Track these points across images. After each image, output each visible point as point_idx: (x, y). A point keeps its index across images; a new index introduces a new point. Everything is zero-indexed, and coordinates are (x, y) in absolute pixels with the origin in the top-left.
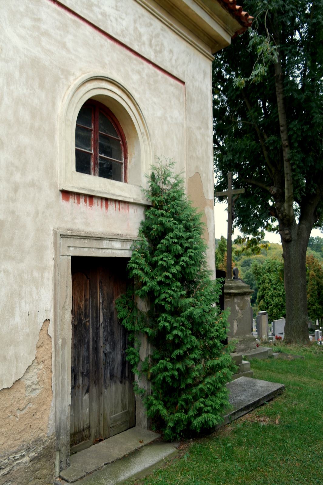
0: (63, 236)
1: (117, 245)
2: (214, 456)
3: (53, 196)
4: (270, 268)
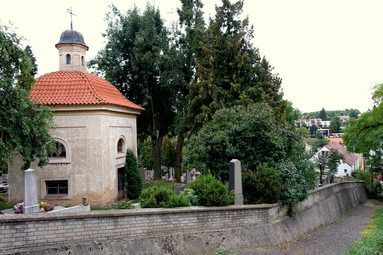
1: (123, 165)
2: (206, 96)
3: (115, 159)
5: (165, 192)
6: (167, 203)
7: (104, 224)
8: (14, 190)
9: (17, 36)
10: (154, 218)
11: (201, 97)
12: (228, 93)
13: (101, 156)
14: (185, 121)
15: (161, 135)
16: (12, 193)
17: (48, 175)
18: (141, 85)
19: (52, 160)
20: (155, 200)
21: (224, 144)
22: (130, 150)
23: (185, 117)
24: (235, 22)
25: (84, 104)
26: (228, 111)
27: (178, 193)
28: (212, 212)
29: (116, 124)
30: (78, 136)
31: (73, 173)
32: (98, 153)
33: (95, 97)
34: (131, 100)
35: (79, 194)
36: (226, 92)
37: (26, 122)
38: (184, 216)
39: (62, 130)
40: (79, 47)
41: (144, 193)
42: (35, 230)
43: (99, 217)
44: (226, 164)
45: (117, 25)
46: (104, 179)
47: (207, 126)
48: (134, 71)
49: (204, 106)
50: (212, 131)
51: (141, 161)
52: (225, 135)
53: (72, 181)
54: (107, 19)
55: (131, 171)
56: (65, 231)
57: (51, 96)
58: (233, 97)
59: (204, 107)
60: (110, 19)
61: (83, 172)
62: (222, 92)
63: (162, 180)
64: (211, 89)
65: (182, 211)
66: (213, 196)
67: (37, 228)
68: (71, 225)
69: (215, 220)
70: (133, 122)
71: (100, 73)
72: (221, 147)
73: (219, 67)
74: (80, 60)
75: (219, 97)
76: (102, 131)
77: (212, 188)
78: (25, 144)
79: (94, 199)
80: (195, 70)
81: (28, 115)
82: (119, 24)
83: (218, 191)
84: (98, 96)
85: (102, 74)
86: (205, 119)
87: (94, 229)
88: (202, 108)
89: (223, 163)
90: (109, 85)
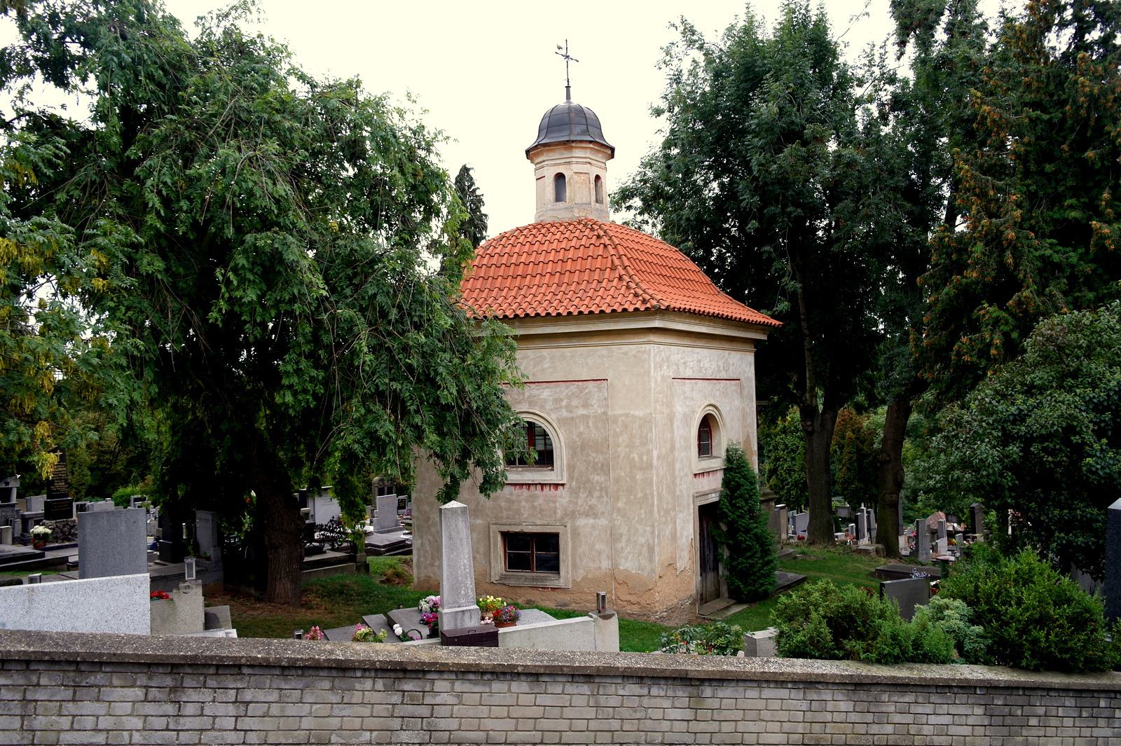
1: (713, 495)
2: (993, 274)
3: (691, 476)
5: (863, 604)
6: (868, 645)
7: (658, 699)
9: (425, 133)
10: (827, 695)
11: (975, 275)
12: (1080, 259)
13: (649, 466)
14: (916, 360)
15: (832, 405)
16: (422, 559)
18: (767, 248)
19: (515, 475)
20: (825, 630)
21: (1076, 439)
22: (737, 450)
23: (916, 346)
24: (1106, 7)
25: (602, 312)
26: (1087, 322)
27: (908, 614)
28: (1045, 693)
30: (586, 405)
31: (573, 515)
32: (641, 459)
33: (632, 291)
34: (737, 295)
36: (1071, 254)
37: (446, 367)
38: (934, 698)
40: (589, 151)
42: (455, 701)
43: (641, 678)
44: (1083, 512)
45: (696, 76)
46: (659, 536)
47: (1005, 374)
48: (745, 208)
49: (986, 305)
50: (1023, 393)
51: (768, 481)
52: (1076, 407)
54: (665, 62)
55: (741, 517)
56: (537, 712)
57: (513, 293)
58: (1100, 271)
59: (988, 311)
60: (675, 62)
62: (1055, 255)
63: (834, 544)
64: (1015, 248)
65: (925, 679)
66: (1048, 634)
67: (459, 695)
68: (554, 694)
69: (1054, 722)
70: (743, 364)
71: (647, 222)
72: (1060, 450)
73: (1043, 169)
75: (1045, 275)
77: (1039, 602)
78: (445, 430)
80: (946, 191)
81: (452, 349)
82: (701, 75)
83: (1067, 617)
84: (641, 288)
85: (653, 227)
86: (993, 351)
87: (626, 713)
88: (977, 313)
89: (1071, 508)
90: (673, 255)
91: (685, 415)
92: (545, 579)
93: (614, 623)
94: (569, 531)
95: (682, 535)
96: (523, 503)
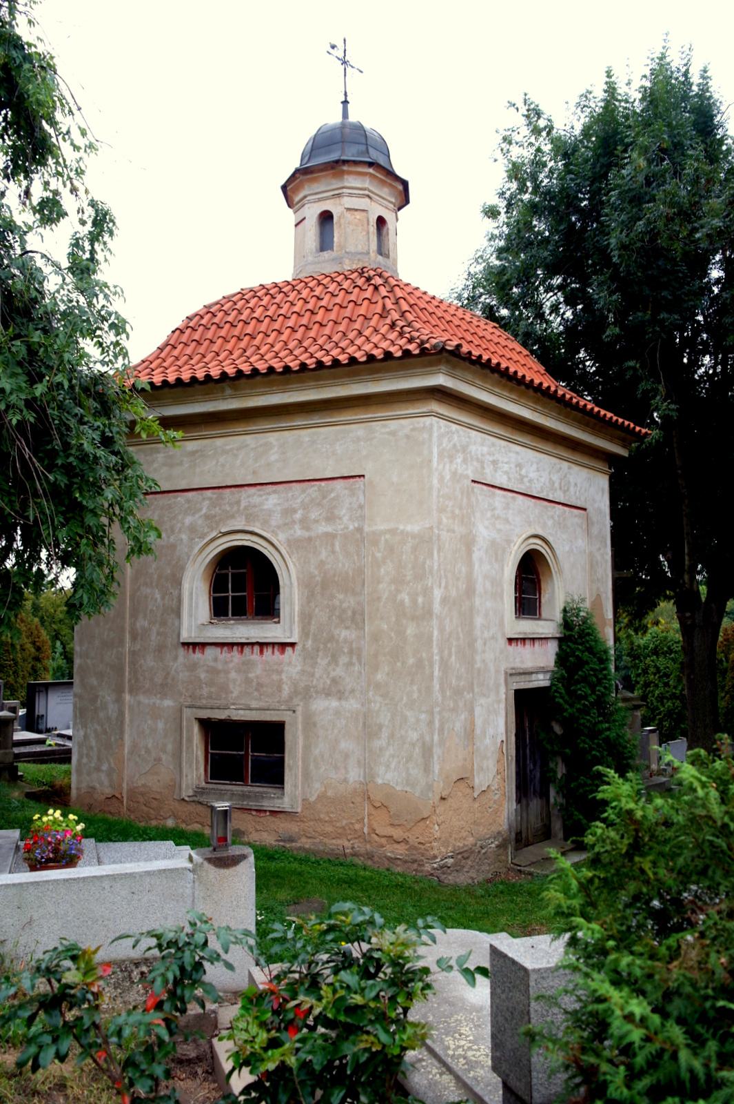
0: (511, 675)
1: (541, 676)
3: (502, 642)
4: (656, 647)
8: (91, 748)
13: (428, 613)
16: (85, 760)
17: (210, 697)
29: (509, 478)
30: (331, 518)
31: (307, 694)
32: (414, 602)
35: (330, 793)
39: (269, 494)
40: (367, 179)
41: (655, 808)
53: (300, 727)
55: (585, 711)
61: (349, 688)
74: (368, 233)
76: (435, 494)
79: (392, 825)
91: (493, 543)
92: (261, 796)
93: (245, 874)
94: (300, 719)
95: (484, 732)
96: (233, 675)
